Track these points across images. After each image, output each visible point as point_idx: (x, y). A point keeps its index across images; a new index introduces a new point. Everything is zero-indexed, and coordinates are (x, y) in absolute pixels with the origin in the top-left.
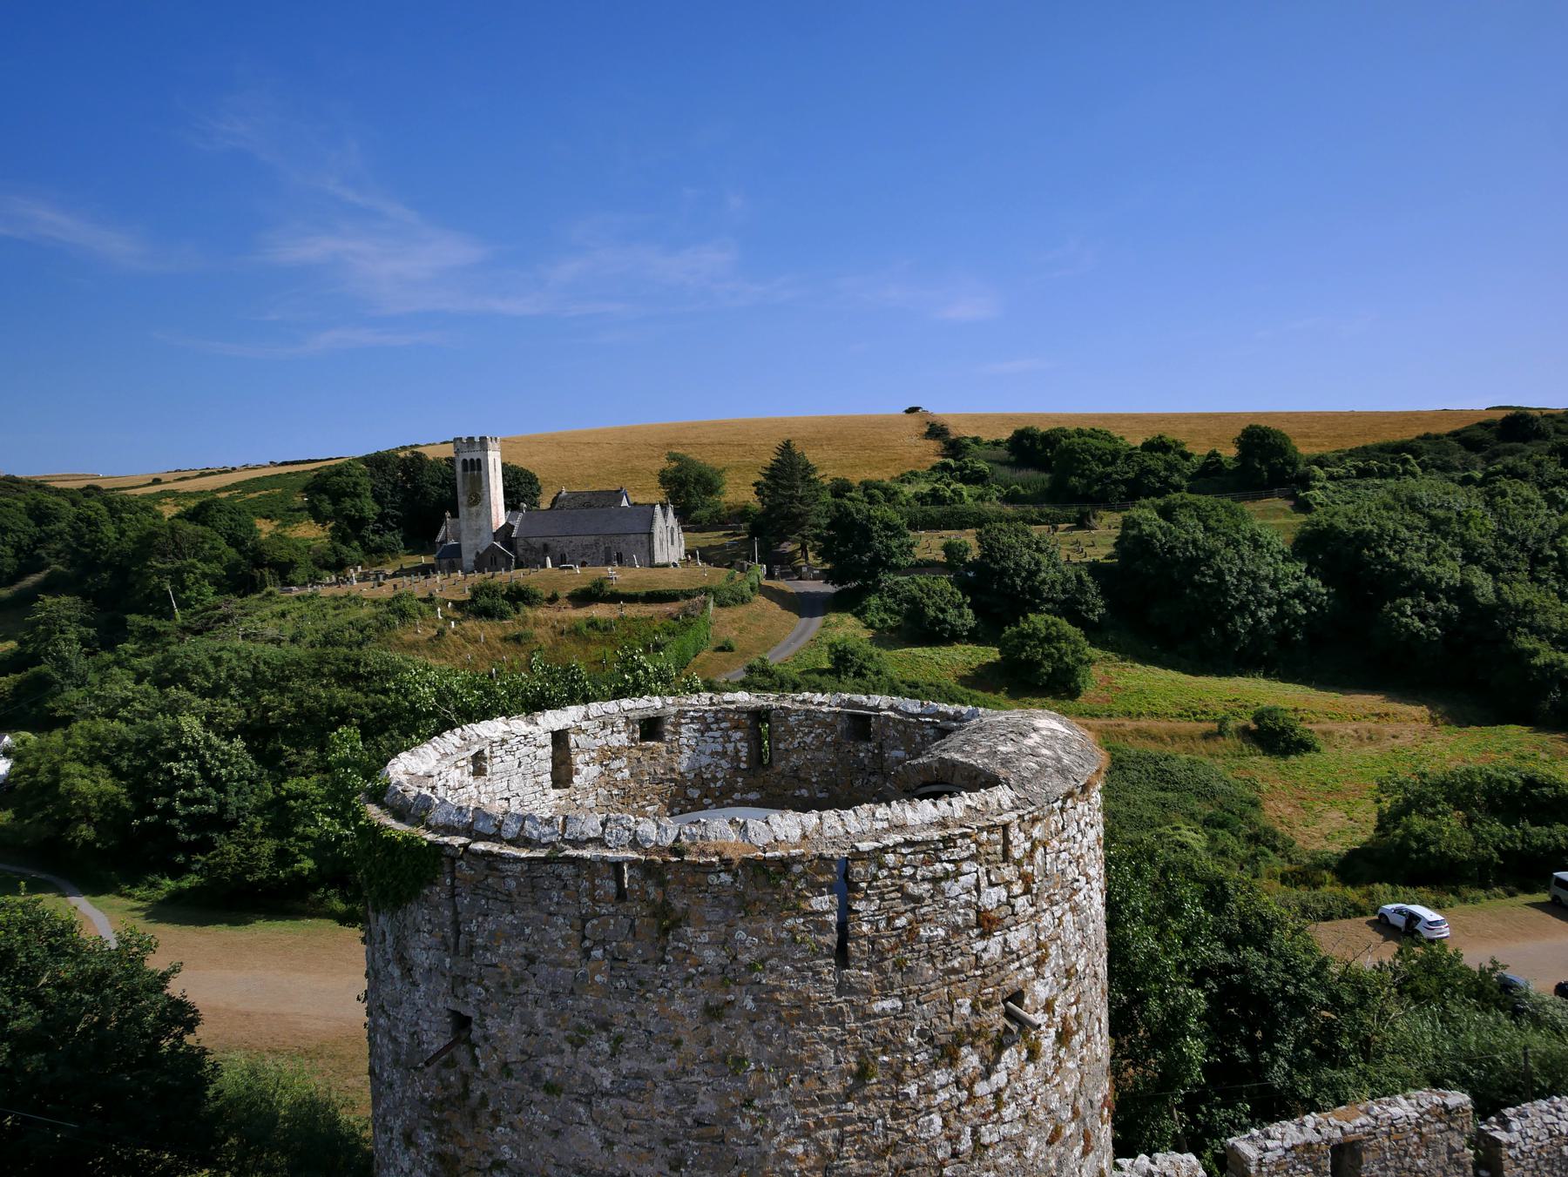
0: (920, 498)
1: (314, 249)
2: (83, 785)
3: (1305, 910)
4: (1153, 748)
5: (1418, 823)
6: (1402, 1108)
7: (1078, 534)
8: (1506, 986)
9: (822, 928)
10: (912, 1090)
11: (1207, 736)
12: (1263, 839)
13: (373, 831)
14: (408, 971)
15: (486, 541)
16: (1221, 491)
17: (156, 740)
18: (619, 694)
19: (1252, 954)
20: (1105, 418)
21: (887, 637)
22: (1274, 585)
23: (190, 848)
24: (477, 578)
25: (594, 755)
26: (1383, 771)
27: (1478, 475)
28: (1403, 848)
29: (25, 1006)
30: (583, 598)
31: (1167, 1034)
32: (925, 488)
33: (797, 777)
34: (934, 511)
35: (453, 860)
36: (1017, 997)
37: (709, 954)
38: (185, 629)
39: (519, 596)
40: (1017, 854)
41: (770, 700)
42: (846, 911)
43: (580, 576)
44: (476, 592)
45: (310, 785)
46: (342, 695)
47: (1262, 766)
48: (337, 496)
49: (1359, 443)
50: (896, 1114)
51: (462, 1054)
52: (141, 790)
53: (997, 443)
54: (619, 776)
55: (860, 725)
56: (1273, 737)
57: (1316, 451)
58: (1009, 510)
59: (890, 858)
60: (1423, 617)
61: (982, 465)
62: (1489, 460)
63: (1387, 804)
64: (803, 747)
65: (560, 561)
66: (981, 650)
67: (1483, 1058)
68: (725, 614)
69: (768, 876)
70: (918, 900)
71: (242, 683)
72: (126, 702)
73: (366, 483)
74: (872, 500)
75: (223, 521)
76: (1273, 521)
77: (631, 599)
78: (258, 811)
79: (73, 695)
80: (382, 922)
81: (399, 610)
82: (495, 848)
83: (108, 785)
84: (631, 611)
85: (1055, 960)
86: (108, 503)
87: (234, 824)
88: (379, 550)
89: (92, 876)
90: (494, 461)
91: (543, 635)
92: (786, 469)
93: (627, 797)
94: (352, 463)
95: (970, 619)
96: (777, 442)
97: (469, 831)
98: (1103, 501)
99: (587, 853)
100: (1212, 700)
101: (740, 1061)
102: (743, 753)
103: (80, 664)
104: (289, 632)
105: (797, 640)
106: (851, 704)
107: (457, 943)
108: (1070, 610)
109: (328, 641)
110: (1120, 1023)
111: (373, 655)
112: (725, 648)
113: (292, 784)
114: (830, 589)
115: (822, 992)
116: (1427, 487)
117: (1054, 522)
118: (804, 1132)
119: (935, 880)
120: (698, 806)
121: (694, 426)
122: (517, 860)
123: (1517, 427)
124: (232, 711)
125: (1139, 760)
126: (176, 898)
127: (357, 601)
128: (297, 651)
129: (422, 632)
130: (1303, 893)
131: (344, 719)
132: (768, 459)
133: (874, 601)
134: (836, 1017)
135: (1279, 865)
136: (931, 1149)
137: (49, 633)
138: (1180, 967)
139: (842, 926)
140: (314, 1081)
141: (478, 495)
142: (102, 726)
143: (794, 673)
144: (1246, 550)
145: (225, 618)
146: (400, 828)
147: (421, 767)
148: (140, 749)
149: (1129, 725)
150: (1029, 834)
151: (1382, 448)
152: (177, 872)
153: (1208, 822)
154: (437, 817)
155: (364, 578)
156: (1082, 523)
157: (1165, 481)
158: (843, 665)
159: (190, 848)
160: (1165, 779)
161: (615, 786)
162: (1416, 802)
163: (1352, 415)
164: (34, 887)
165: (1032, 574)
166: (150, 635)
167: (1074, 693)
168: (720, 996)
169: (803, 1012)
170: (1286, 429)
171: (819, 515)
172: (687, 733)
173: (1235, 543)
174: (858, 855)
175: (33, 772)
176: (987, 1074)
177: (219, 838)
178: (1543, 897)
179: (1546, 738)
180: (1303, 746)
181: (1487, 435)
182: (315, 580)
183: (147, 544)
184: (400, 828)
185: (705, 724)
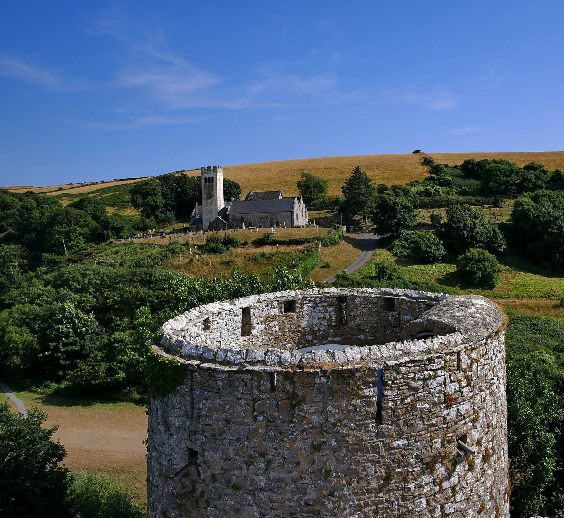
0: (419, 193)
4: (529, 313)
7: (494, 210)
9: (370, 404)
10: (412, 486)
11: (555, 307)
13: (154, 358)
14: (168, 428)
15: (215, 216)
18: (275, 289)
21: (403, 261)
25: (262, 319)
30: (259, 243)
31: (536, 457)
32: (422, 188)
33: (359, 329)
34: (426, 199)
35: (192, 372)
36: (463, 438)
37: (315, 418)
38: (70, 260)
39: (229, 242)
40: (464, 366)
41: (347, 292)
42: (381, 395)
43: (258, 232)
44: (208, 241)
45: (125, 336)
50: (404, 499)
51: (192, 470)
52: (44, 339)
54: (273, 330)
55: (389, 303)
58: (461, 199)
59: (403, 369)
61: (449, 178)
64: (362, 314)
68: (327, 250)
69: (344, 377)
70: (416, 389)
71: (96, 286)
73: (159, 189)
74: (397, 194)
75: (91, 208)
77: (282, 243)
78: (100, 349)
79: (14, 292)
80: (157, 404)
81: (172, 249)
82: (213, 366)
83: (28, 337)
84: (282, 249)
86: (36, 200)
88: (163, 221)
92: (357, 181)
93: (277, 340)
96: (353, 168)
98: (505, 194)
99: (257, 368)
100: (557, 289)
101: (328, 472)
102: (333, 318)
103: (18, 277)
104: (119, 261)
105: (360, 262)
106: (386, 293)
107: (193, 414)
108: (490, 246)
109: (138, 265)
110: (514, 450)
111: (158, 272)
112: (326, 266)
113: (116, 335)
114: (377, 237)
117: (482, 204)
119: (424, 380)
120: (311, 344)
122: (223, 372)
124: (90, 299)
125: (523, 319)
126: (57, 392)
127: (152, 245)
128: (122, 270)
129: (182, 260)
131: (143, 303)
132: (348, 175)
133: (397, 243)
134: (375, 449)
139: (379, 403)
140: (119, 485)
141: (211, 194)
143: (358, 278)
145: (89, 255)
147: (177, 326)
148: (44, 319)
149: (518, 302)
152: (59, 380)
153: (556, 349)
154: (186, 351)
155: (156, 234)
156: (495, 205)
157: (534, 184)
158: (382, 274)
160: (535, 328)
165: (472, 229)
166: (53, 263)
167: (492, 287)
168: (319, 439)
171: (372, 202)
172: (307, 308)
174: (387, 368)
176: (448, 478)
177: (80, 362)
182: (132, 236)
183: (54, 219)
185: (315, 304)
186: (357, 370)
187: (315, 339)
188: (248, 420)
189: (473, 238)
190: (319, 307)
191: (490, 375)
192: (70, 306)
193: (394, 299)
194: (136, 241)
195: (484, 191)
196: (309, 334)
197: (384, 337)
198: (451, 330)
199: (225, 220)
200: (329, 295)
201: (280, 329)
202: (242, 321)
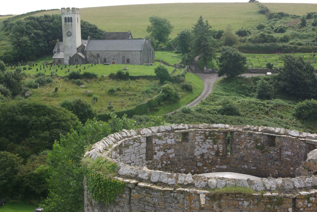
25: (161, 147)
33: (243, 160)
35: (130, 189)
39: (89, 76)
43: (114, 69)
53: (294, 17)
54: (171, 156)
102: (221, 149)
106: (265, 131)
122: (158, 191)
161: (169, 160)
187: (205, 166)
190: (208, 139)
193: (275, 136)
196: (200, 162)
197: (266, 168)
200: (217, 130)
201: (176, 156)
202: (146, 148)
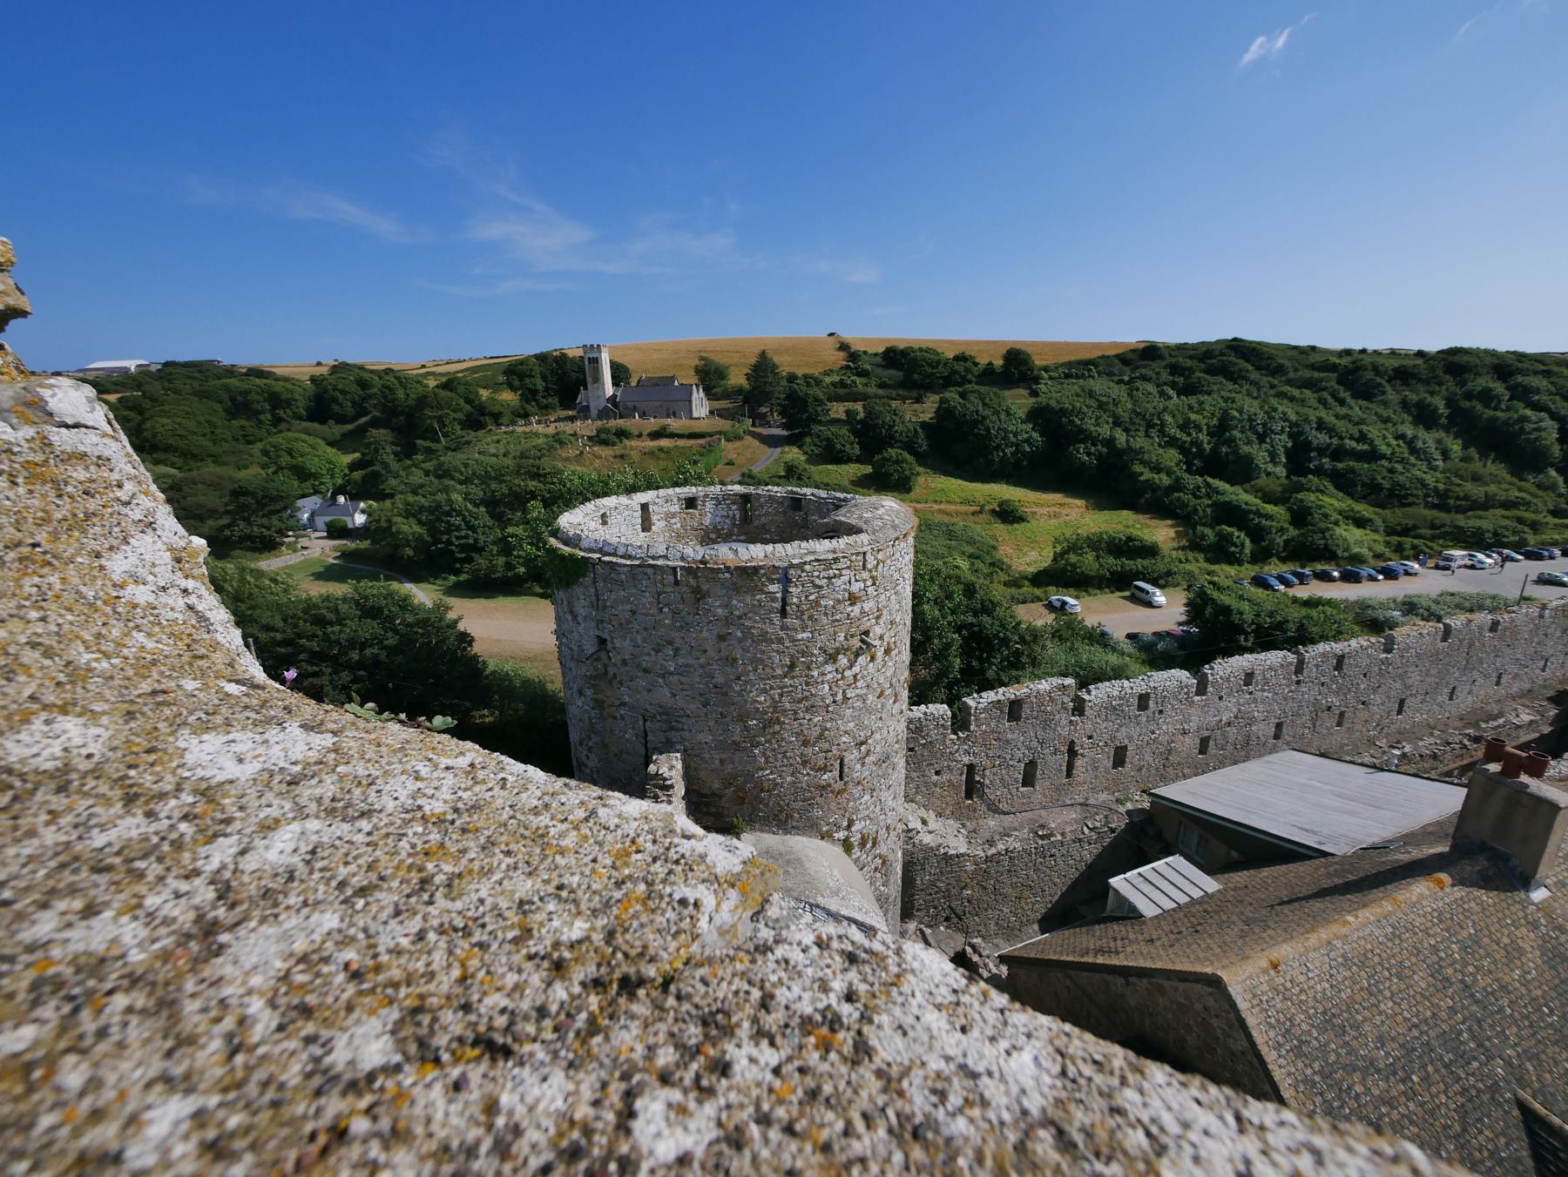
0: (834, 384)
1: (494, 230)
2: (405, 528)
3: (1013, 598)
4: (947, 519)
5: (1073, 558)
6: (1044, 686)
7: (916, 406)
8: (1103, 634)
9: (774, 600)
10: (815, 673)
11: (974, 514)
12: (997, 565)
13: (554, 550)
14: (575, 617)
15: (603, 403)
16: (992, 383)
17: (439, 506)
18: (676, 484)
19: (985, 619)
20: (935, 341)
21: (814, 459)
22: (1015, 435)
23: (462, 561)
24: (599, 423)
26: (1057, 533)
27: (1126, 378)
28: (1064, 570)
29: (390, 634)
30: (655, 435)
31: (941, 655)
32: (837, 378)
33: (764, 528)
34: (841, 391)
36: (866, 633)
37: (720, 611)
38: (448, 449)
39: (622, 434)
40: (869, 566)
41: (751, 490)
42: (785, 592)
43: (653, 423)
44: (599, 431)
45: (519, 531)
46: (532, 484)
47: (1000, 528)
48: (521, 377)
49: (1067, 359)
50: (807, 684)
51: (603, 655)
52: (433, 531)
55: (796, 503)
56: (1008, 515)
57: (1044, 363)
58: (881, 392)
59: (807, 567)
60: (1088, 455)
61: (867, 367)
62: (1133, 371)
63: (1058, 549)
64: (768, 514)
65: (643, 415)
66: (862, 467)
67: (1087, 667)
68: (730, 445)
69: (748, 575)
70: (821, 587)
71: (480, 477)
72: (422, 486)
73: (537, 369)
74: (808, 385)
75: (461, 389)
76: (1018, 401)
77: (681, 436)
78: (494, 543)
79: (393, 482)
80: (561, 594)
81: (559, 440)
82: (614, 560)
83: (417, 529)
84: (681, 443)
85: (885, 617)
86: (398, 378)
87: (483, 549)
88: (546, 407)
89: (417, 574)
90: (605, 358)
91: (635, 456)
92: (763, 367)
93: (679, 537)
94: (527, 358)
95: (857, 450)
96: (757, 351)
97: (600, 551)
98: (930, 388)
99: (659, 563)
100: (978, 495)
101: (735, 660)
103: (394, 466)
104: (502, 451)
105: (767, 459)
106: (792, 492)
107: (597, 603)
108: (910, 447)
109: (523, 456)
110: (917, 648)
111: (546, 464)
112: (730, 463)
113: (510, 530)
114: (785, 433)
115: (774, 627)
116: (1099, 385)
117: (904, 399)
118: (765, 691)
119: (829, 578)
120: (714, 542)
121: (712, 341)
123: (1150, 352)
124: (477, 491)
125: (939, 525)
126: (457, 585)
127: (537, 435)
128: (508, 461)
129: (572, 452)
130: (1013, 590)
131: (534, 497)
132: (753, 361)
133: (808, 440)
134: (780, 641)
135: (1003, 577)
136: (823, 699)
137: (377, 451)
138: (949, 624)
139: (784, 600)
140: (531, 672)
141: (597, 379)
142: (411, 498)
143: (765, 477)
144: (1003, 417)
145: (468, 443)
146: (567, 550)
147: (569, 520)
148: (431, 510)
149: (936, 507)
150: (877, 556)
151: (1079, 363)
152: (457, 572)
153: (971, 556)
154: (584, 544)
155: (539, 422)
156: (918, 400)
157: (963, 378)
158: (791, 473)
159: (462, 561)
160: (950, 534)
162: (1073, 547)
163: (1067, 344)
164: (387, 579)
165: (891, 427)
166: (429, 451)
167: (909, 490)
168: (724, 631)
169: (764, 638)
170: (1030, 350)
171: (780, 393)
172: (709, 506)
173: (996, 413)
174: (792, 566)
175: (378, 521)
176: (851, 667)
177: (476, 556)
178: (1127, 594)
179: (1140, 517)
180: (1021, 519)
181: (1134, 356)
182: (513, 423)
183: (422, 401)
184: (567, 550)
185: (718, 501)
186: (761, 567)
188: (654, 611)
189: (892, 437)
191: (897, 575)
192: (456, 497)
194: (519, 429)
195: (907, 384)
198: (859, 531)
199: (615, 408)
